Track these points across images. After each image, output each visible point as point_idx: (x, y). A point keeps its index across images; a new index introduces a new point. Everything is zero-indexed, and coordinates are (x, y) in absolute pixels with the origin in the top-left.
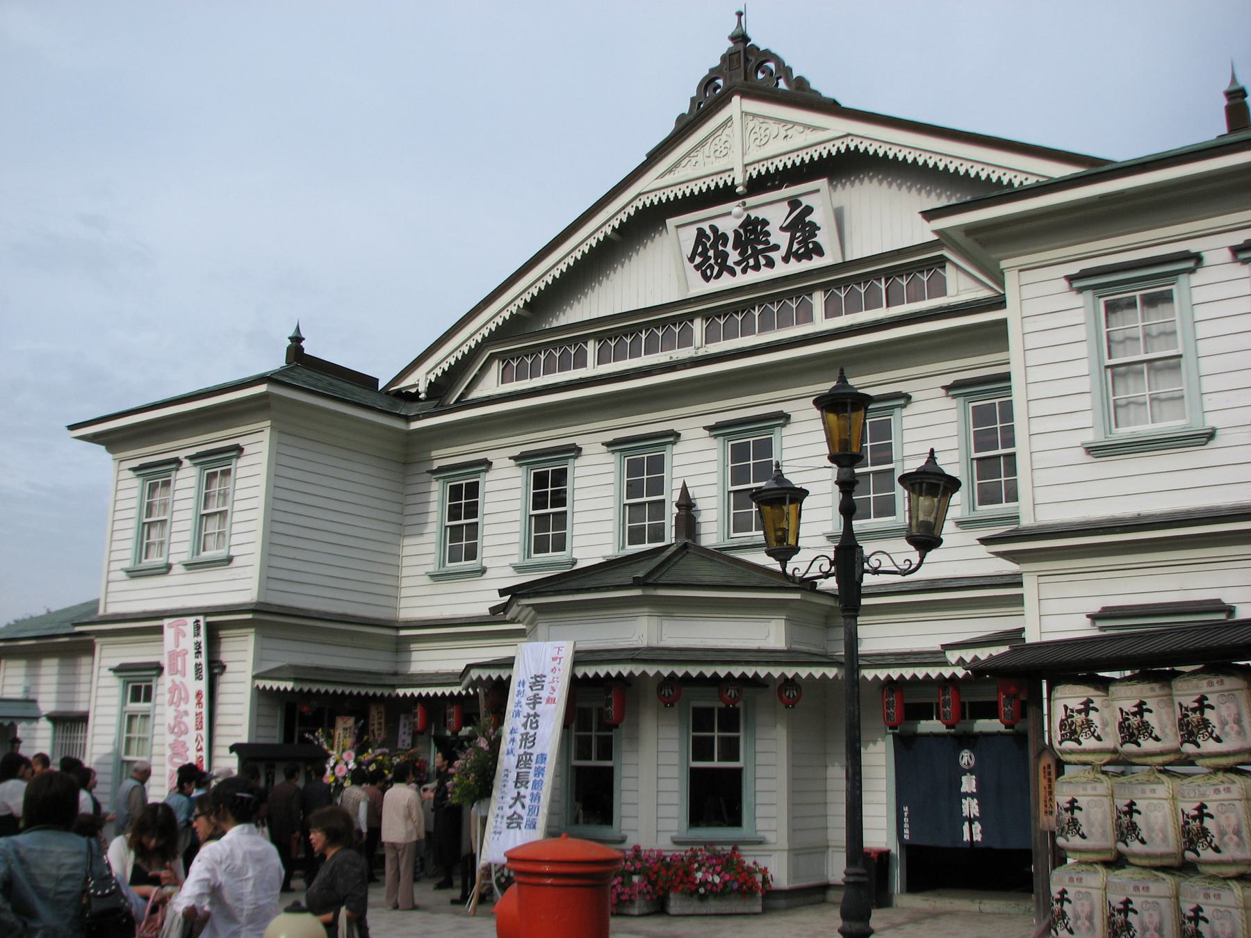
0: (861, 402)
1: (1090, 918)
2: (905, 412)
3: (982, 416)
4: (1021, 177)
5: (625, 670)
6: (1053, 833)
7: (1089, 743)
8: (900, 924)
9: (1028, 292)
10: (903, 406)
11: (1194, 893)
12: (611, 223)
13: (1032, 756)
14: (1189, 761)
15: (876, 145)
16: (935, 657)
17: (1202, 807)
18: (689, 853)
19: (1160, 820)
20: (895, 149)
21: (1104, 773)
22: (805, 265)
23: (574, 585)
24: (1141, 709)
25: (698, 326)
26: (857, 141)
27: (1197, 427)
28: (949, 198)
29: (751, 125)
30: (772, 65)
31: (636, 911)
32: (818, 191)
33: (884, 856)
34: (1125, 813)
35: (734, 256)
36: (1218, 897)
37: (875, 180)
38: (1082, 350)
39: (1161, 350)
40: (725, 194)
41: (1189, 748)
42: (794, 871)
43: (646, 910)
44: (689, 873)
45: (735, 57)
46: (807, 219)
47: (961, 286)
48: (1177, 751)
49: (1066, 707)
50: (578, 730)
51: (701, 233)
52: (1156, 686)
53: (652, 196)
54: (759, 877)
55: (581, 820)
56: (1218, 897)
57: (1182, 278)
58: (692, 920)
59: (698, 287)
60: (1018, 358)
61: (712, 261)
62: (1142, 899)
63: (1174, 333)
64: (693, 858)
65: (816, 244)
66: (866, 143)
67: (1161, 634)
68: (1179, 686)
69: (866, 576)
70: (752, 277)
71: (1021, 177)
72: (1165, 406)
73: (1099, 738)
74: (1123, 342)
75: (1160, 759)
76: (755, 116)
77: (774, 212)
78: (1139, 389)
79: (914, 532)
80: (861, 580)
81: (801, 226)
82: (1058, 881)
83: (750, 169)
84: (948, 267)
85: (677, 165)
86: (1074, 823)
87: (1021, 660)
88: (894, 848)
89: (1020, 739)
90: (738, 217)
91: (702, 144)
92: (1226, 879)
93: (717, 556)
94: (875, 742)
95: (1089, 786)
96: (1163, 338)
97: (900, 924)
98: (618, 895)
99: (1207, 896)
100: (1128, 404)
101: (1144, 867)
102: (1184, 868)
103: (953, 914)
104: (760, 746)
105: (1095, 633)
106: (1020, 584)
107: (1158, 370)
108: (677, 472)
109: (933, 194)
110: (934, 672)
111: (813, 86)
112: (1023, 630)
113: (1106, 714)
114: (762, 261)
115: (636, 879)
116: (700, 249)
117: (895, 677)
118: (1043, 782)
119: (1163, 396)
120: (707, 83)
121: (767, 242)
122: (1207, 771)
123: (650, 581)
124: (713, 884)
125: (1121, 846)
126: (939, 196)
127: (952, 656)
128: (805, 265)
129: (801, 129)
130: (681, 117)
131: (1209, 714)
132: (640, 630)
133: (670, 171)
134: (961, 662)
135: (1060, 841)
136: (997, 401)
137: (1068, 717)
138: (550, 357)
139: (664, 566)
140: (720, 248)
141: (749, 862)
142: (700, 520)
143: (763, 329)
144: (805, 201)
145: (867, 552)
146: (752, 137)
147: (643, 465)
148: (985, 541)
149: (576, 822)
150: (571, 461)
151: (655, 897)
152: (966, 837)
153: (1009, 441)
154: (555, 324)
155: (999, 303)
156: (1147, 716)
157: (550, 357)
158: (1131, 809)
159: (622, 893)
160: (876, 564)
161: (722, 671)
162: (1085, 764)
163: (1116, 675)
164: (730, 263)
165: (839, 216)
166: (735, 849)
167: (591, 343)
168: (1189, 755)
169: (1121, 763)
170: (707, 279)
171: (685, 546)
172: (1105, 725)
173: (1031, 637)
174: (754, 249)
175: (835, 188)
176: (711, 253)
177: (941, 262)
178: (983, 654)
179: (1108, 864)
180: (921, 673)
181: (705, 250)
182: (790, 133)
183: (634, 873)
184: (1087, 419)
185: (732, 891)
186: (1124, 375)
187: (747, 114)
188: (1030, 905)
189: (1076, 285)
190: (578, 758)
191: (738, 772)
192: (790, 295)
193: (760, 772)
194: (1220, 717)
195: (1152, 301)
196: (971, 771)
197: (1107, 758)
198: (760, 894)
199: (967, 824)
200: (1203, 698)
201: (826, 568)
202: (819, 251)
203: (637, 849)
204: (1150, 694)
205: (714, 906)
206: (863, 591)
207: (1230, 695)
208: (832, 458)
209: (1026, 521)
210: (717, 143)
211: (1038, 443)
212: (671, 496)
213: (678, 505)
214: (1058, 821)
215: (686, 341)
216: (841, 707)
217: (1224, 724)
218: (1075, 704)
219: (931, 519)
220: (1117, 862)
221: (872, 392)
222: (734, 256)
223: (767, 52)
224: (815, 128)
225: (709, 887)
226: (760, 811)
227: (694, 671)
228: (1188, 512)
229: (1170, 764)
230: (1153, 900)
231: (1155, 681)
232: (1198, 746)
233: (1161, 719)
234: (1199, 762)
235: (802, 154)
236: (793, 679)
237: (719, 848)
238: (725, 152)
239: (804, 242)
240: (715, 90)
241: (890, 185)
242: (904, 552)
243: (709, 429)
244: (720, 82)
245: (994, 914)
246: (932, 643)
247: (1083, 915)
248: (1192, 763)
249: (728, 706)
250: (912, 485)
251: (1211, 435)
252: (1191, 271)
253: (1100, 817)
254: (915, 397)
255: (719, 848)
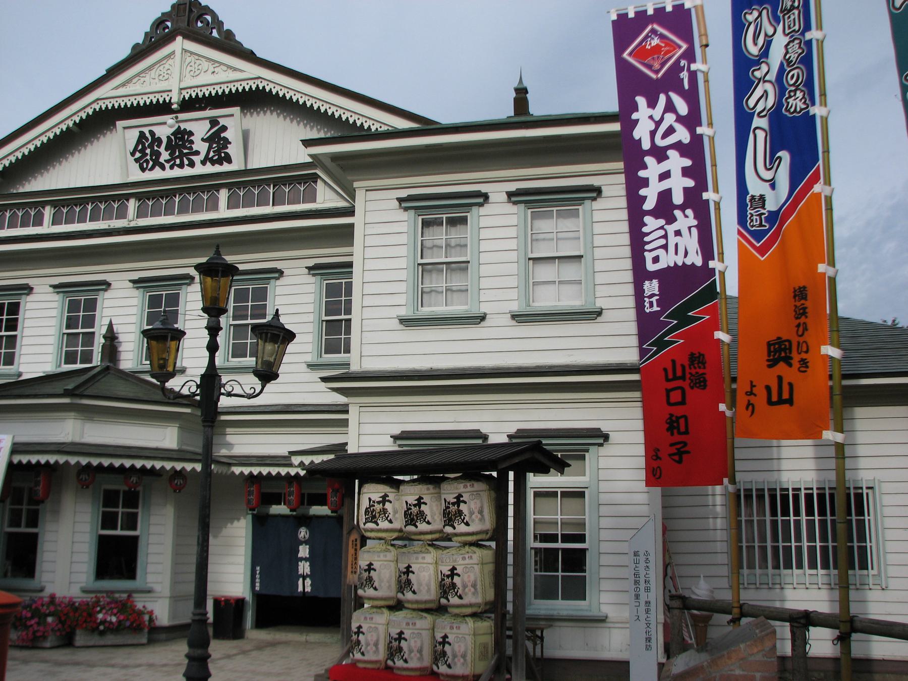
0: (231, 270)
1: (376, 645)
2: (278, 282)
3: (332, 291)
4: (377, 125)
5: (52, 459)
6: (356, 587)
7: (384, 524)
8: (250, 651)
9: (371, 206)
10: (277, 279)
11: (444, 626)
12: (73, 118)
13: (345, 532)
14: (448, 538)
15: (278, 88)
16: (284, 461)
17: (454, 569)
18: (94, 600)
19: (427, 578)
20: (292, 93)
21: (393, 545)
22: (217, 169)
23: (17, 392)
24: (420, 502)
25: (132, 205)
26: (265, 83)
27: (475, 311)
28: (326, 133)
29: (189, 59)
30: (209, 18)
31: (48, 645)
32: (232, 115)
33: (240, 602)
34: (404, 573)
35: (165, 156)
36: (458, 628)
37: (275, 113)
38: (403, 251)
39: (455, 257)
40: (162, 108)
41: (449, 529)
42: (173, 614)
43: (56, 644)
44: (91, 615)
45: (182, 7)
46: (222, 135)
47: (326, 197)
48: (441, 531)
49: (370, 499)
50: (12, 504)
51: (142, 134)
52: (431, 487)
53: (107, 102)
54: (147, 617)
55: (9, 574)
56: (458, 628)
57: (475, 209)
58: (93, 651)
59: (137, 175)
60: (358, 253)
61: (148, 157)
62: (368, 625)
63: (466, 246)
64: (97, 603)
65: (227, 154)
66: (271, 86)
67: (437, 451)
68: (445, 486)
69: (222, 397)
70: (177, 173)
71: (377, 125)
72: (455, 295)
73: (390, 521)
74: (431, 248)
75: (429, 537)
76: (192, 53)
77: (198, 127)
78: (438, 282)
79: (259, 367)
80: (218, 400)
81: (217, 140)
82: (357, 619)
83: (184, 92)
84: (319, 181)
85: (129, 81)
86: (370, 579)
87: (344, 464)
88: (248, 597)
89: (339, 520)
90: (171, 127)
91: (150, 68)
92: (464, 616)
93: (131, 377)
94: (238, 519)
95: (382, 555)
96: (458, 248)
97: (250, 651)
98: (34, 632)
99: (452, 628)
100: (431, 291)
101: (414, 610)
102: (439, 610)
103: (287, 643)
104: (153, 519)
105: (396, 448)
106: (347, 412)
107: (453, 270)
108: (106, 312)
109: (315, 129)
110: (283, 471)
111: (237, 38)
112: (346, 444)
113: (397, 505)
114: (186, 162)
115: (50, 619)
116: (140, 147)
117: (255, 473)
118: (351, 551)
119: (454, 288)
120: (159, 23)
121: (191, 148)
122: (459, 545)
123: (77, 392)
124: (111, 622)
125: (400, 595)
126: (319, 131)
127: (296, 460)
128: (217, 169)
129: (225, 68)
130: (136, 46)
131: (463, 507)
132: (67, 429)
133: (123, 85)
134: (301, 464)
135: (360, 592)
136: (344, 281)
137: (370, 506)
138: (14, 216)
139: (88, 383)
140: (156, 148)
141: (139, 606)
142: (120, 349)
143: (180, 212)
144: (222, 122)
145: (224, 380)
146: (186, 69)
147: (81, 305)
148: (324, 379)
149: (5, 575)
150: (24, 297)
151: (64, 633)
152: (300, 589)
153: (348, 311)
154: (21, 190)
155: (349, 212)
156: (423, 507)
157: (14, 216)
158: (408, 570)
159: (38, 631)
160: (230, 389)
161: (128, 463)
162: (380, 539)
163: (407, 478)
164: (162, 160)
165: (246, 136)
166: (129, 596)
167: (48, 208)
168: (448, 534)
169: (404, 539)
170: (143, 170)
171: (108, 368)
172: (395, 512)
173: (352, 449)
174: (180, 152)
175: (245, 115)
176: (148, 151)
177: (315, 178)
178: (318, 459)
179: (391, 608)
180: (274, 471)
181: (144, 148)
182: (216, 70)
183: (49, 615)
184: (402, 299)
185: (125, 628)
186: (430, 271)
187: (186, 51)
188: (337, 637)
189: (404, 205)
190: (11, 526)
191: (135, 539)
192: (203, 189)
193: (152, 539)
194: (469, 509)
195: (452, 222)
196: (306, 542)
197: (395, 535)
198: (146, 630)
199: (301, 580)
200: (460, 496)
201: (193, 389)
202: (228, 159)
203: (52, 597)
204: (426, 492)
205: (110, 639)
206: (219, 410)
207: (477, 494)
208: (204, 310)
209: (355, 368)
210: (162, 70)
211: (367, 313)
212: (100, 330)
213: (104, 337)
214: (360, 579)
215: (122, 215)
216: (204, 491)
217: (471, 513)
218: (376, 497)
219: (272, 360)
220: (397, 606)
221: (241, 267)
222: (165, 156)
223: (207, 7)
224: (235, 69)
225: (107, 625)
226: (150, 568)
227: (106, 462)
228: (464, 369)
229: (436, 540)
230: (418, 633)
231: (430, 483)
232: (454, 528)
233: (432, 510)
234: (454, 539)
235: (224, 87)
236: (180, 471)
237: (117, 595)
238: (166, 77)
239: (218, 152)
240: (164, 29)
241: (285, 118)
242: (251, 382)
243: (134, 282)
244: (169, 24)
245: (315, 643)
246: (282, 450)
247: (372, 643)
248: (450, 540)
249: (130, 489)
250: (261, 334)
251: (483, 318)
252: (481, 205)
253: (388, 575)
254: (286, 272)
255: (117, 595)
